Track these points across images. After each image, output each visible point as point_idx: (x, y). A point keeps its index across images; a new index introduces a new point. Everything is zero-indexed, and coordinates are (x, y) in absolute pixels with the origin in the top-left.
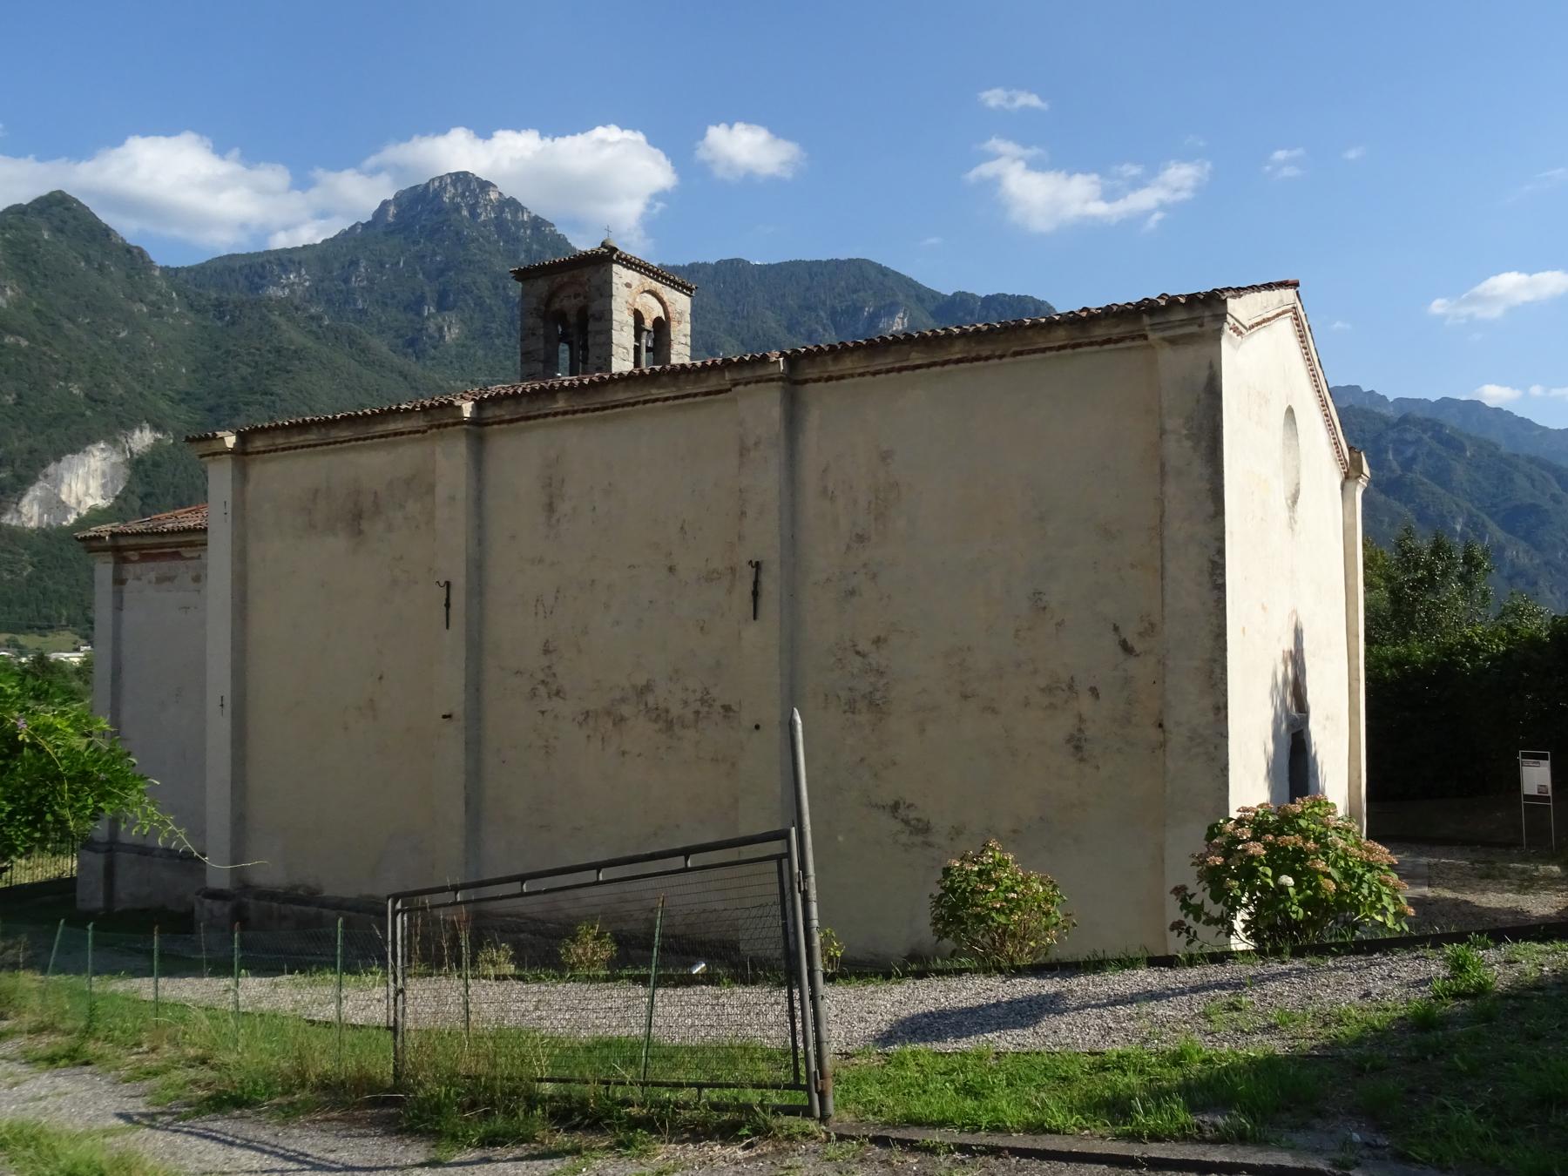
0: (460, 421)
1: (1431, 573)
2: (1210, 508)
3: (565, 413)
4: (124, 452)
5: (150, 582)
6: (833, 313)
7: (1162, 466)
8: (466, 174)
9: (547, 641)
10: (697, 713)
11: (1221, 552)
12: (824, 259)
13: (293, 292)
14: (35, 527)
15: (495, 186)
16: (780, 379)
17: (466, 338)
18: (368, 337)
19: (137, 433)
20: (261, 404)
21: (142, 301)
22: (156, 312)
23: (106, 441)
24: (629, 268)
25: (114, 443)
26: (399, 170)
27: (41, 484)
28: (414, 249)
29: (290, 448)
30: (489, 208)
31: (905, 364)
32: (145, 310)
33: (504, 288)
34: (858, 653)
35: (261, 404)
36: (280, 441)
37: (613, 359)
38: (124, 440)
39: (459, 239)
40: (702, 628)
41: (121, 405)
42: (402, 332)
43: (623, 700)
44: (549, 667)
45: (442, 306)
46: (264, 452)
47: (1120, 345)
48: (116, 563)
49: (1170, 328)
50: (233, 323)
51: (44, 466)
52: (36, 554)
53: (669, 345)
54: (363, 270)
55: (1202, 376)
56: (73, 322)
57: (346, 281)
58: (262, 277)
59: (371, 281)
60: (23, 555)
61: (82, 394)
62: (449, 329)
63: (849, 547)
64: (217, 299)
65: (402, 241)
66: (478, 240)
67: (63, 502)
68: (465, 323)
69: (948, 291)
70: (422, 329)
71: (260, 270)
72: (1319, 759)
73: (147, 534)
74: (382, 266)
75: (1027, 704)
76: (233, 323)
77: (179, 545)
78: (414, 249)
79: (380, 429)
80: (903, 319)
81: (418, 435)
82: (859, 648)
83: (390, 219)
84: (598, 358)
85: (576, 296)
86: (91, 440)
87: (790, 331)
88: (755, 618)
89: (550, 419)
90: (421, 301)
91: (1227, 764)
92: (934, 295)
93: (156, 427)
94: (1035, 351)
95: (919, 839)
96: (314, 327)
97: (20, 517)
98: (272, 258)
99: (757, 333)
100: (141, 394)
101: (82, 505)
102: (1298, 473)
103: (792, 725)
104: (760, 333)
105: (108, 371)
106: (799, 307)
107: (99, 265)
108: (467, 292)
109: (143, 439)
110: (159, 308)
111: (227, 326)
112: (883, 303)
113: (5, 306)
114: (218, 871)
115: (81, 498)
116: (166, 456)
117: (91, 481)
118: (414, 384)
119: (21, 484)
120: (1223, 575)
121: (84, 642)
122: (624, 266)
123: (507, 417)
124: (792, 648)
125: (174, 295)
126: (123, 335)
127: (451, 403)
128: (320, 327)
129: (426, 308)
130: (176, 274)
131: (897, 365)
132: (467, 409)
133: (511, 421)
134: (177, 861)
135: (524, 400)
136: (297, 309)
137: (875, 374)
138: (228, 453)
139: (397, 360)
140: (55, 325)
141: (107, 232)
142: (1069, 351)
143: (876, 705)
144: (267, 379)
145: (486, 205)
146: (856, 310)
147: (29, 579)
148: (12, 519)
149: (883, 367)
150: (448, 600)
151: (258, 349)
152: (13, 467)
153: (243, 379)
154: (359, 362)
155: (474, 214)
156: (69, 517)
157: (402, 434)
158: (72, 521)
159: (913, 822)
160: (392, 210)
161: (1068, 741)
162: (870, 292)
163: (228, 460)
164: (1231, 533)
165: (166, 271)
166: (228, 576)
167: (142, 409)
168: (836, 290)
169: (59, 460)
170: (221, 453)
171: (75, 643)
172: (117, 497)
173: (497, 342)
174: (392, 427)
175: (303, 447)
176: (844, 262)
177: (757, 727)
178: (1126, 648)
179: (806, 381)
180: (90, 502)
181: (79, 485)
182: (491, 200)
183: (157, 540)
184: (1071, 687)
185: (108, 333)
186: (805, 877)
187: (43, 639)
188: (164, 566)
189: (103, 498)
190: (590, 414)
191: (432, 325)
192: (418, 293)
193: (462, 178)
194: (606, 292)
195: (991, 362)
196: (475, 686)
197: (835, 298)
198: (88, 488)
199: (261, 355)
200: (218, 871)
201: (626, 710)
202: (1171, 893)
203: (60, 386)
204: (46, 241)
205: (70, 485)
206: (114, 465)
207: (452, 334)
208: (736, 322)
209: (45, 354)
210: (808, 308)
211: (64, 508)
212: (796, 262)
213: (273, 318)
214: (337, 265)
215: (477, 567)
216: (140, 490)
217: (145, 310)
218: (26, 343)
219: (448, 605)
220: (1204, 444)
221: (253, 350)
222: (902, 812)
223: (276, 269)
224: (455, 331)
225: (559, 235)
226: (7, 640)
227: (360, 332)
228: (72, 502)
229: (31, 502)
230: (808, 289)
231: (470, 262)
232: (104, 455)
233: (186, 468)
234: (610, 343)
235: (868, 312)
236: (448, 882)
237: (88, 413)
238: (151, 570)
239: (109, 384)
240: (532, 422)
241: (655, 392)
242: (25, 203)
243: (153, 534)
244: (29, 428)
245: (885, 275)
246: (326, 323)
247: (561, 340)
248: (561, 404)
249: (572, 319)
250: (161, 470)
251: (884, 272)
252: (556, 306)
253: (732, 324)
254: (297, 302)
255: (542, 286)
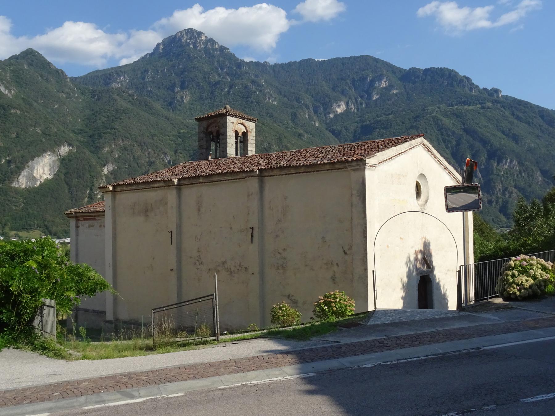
0: (174, 185)
1: (531, 215)
2: (363, 215)
3: (202, 183)
4: (57, 155)
5: (86, 227)
6: (353, 81)
7: (352, 203)
8: (191, 29)
9: (199, 249)
10: (238, 269)
11: (366, 227)
12: (349, 56)
13: (122, 85)
14: (24, 188)
15: (203, 34)
16: (257, 176)
17: (193, 100)
18: (153, 103)
19: (62, 147)
20: (110, 133)
21: (63, 92)
22: (69, 97)
23: (51, 151)
24: (233, 117)
25: (53, 152)
26: (163, 27)
27: (26, 170)
28: (171, 63)
29: (127, 190)
30: (201, 43)
31: (289, 173)
32: (64, 96)
33: (209, 78)
34: (279, 253)
35: (110, 133)
36: (125, 188)
37: (228, 148)
38: (57, 151)
39: (189, 58)
40: (239, 245)
41: (56, 136)
42: (166, 99)
43: (219, 266)
44: (199, 256)
45: (183, 87)
46: (120, 191)
47: (343, 170)
48: (76, 221)
49: (353, 167)
50: (99, 99)
51: (27, 163)
52: (25, 198)
53: (248, 141)
54: (150, 74)
55: (361, 180)
56: (37, 102)
57: (144, 79)
58: (110, 79)
59: (153, 78)
60: (20, 199)
61: (41, 132)
62: (186, 97)
63: (276, 223)
64: (92, 89)
65: (166, 60)
66: (197, 57)
67: (35, 177)
68: (192, 94)
69: (407, 67)
70: (174, 98)
71: (109, 76)
72: (442, 284)
73: (86, 212)
74: (158, 71)
75: (321, 268)
76: (99, 99)
77: (95, 216)
78: (171, 63)
79: (152, 186)
80: (386, 82)
81: (163, 188)
82: (280, 252)
83: (161, 51)
84: (223, 148)
85: (216, 127)
86: (45, 151)
87: (334, 90)
88: (252, 243)
89: (198, 184)
90: (174, 86)
91: (367, 285)
92: (400, 70)
93: (70, 145)
94: (322, 171)
95: (295, 305)
96: (131, 98)
97: (19, 184)
98: (113, 71)
99: (319, 92)
100: (63, 131)
101: (42, 179)
102: (428, 193)
103: (215, 276)
104: (320, 91)
105: (50, 122)
106: (338, 79)
107: (46, 78)
108: (193, 81)
109: (64, 150)
110: (70, 95)
111: (96, 101)
112: (376, 75)
113: (11, 97)
114: (110, 317)
115: (42, 175)
116: (74, 157)
117: (45, 168)
118: (171, 122)
119: (19, 169)
120: (366, 234)
121: (44, 234)
122: (231, 116)
123: (187, 183)
124: (262, 251)
125: (75, 89)
126: (56, 106)
127: (171, 180)
128: (133, 99)
129: (176, 88)
130: (76, 80)
131: (288, 173)
132: (176, 181)
133: (188, 185)
134: (96, 313)
135: (191, 179)
136: (124, 92)
137: (282, 175)
138: (110, 192)
139: (165, 113)
140: (31, 105)
141: (49, 64)
142: (330, 171)
143: (284, 267)
144: (113, 123)
145: (200, 42)
146: (364, 79)
147: (23, 209)
148: (15, 185)
149: (284, 173)
150: (171, 236)
151: (109, 110)
152: (16, 163)
153: (103, 123)
154: (149, 114)
155: (195, 47)
156: (37, 183)
157: (158, 187)
158: (38, 185)
159: (293, 300)
160: (161, 47)
161: (331, 278)
162: (370, 70)
163: (110, 195)
164: (370, 222)
165: (72, 78)
166: (111, 227)
167: (64, 137)
168: (355, 70)
169: (33, 160)
170: (108, 192)
171: (40, 235)
172: (55, 174)
173: (206, 102)
174: (156, 185)
175: (131, 190)
176: (358, 57)
177: (253, 274)
178: (345, 253)
179: (265, 176)
180: (45, 177)
181: (41, 170)
182: (202, 40)
183: (88, 214)
184: (332, 263)
185: (50, 106)
186: (216, 301)
187: (28, 233)
188: (91, 222)
189: (50, 175)
190: (209, 183)
191: (179, 96)
192: (173, 82)
193: (190, 31)
194: (225, 126)
195: (311, 173)
196: (179, 261)
197: (354, 74)
198: (44, 171)
199: (110, 113)
200: (110, 317)
201: (220, 268)
202: (312, 312)
203: (33, 129)
204: (26, 70)
205: (37, 170)
206: (54, 161)
207: (187, 99)
208: (309, 87)
209: (26, 116)
210: (342, 79)
211: (35, 179)
212: (336, 58)
213: (114, 96)
214: (139, 72)
215: (179, 226)
216: (64, 171)
217: (64, 96)
218: (20, 112)
219: (171, 238)
220: (361, 198)
221: (106, 111)
222: (291, 297)
223: (115, 76)
224: (188, 98)
225: (232, 53)
226: (15, 234)
227: (149, 101)
228: (38, 177)
229: (23, 179)
230: (342, 70)
231: (194, 67)
232: (50, 157)
233: (81, 161)
234: (227, 143)
235: (370, 79)
236: (162, 306)
237: (44, 140)
238: (87, 223)
239: (51, 128)
240: (193, 185)
241: (226, 178)
242: (18, 54)
243: (87, 212)
244: (21, 147)
245: (377, 62)
246: (136, 97)
247: (211, 141)
248: (201, 180)
249: (215, 134)
250: (72, 162)
251: (377, 60)
252: (210, 130)
253: (308, 89)
254: (124, 89)
255: (205, 123)
